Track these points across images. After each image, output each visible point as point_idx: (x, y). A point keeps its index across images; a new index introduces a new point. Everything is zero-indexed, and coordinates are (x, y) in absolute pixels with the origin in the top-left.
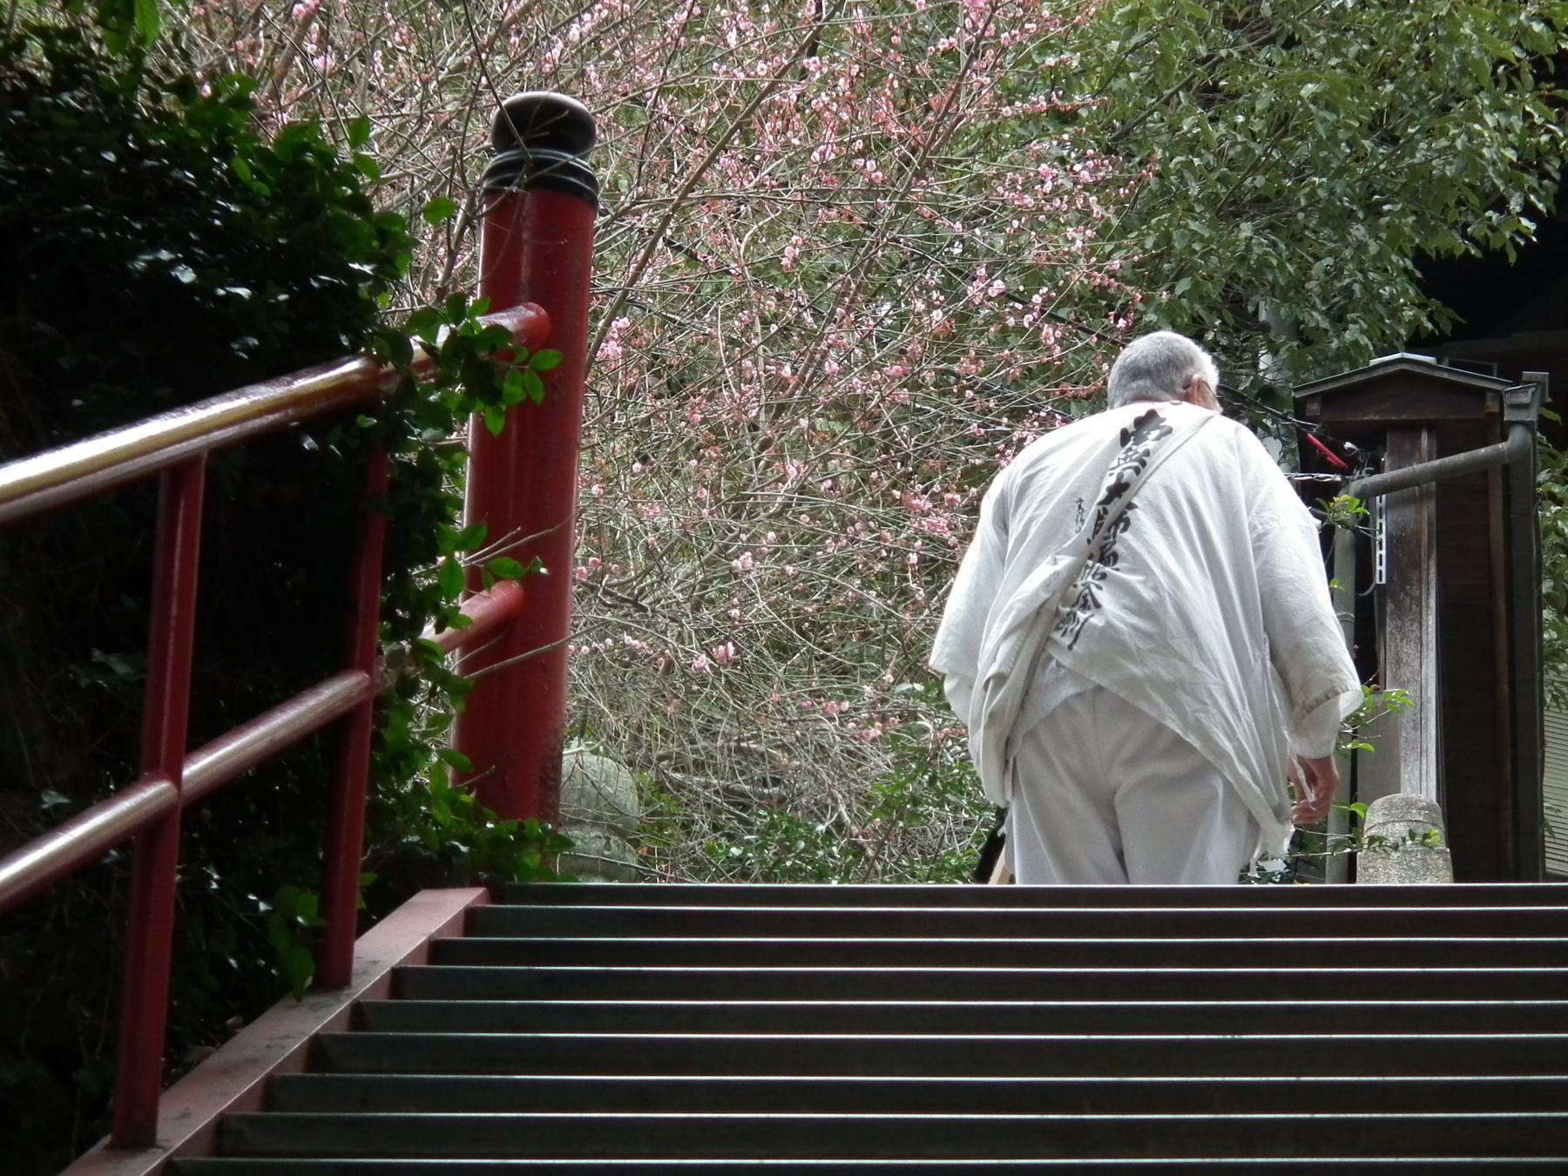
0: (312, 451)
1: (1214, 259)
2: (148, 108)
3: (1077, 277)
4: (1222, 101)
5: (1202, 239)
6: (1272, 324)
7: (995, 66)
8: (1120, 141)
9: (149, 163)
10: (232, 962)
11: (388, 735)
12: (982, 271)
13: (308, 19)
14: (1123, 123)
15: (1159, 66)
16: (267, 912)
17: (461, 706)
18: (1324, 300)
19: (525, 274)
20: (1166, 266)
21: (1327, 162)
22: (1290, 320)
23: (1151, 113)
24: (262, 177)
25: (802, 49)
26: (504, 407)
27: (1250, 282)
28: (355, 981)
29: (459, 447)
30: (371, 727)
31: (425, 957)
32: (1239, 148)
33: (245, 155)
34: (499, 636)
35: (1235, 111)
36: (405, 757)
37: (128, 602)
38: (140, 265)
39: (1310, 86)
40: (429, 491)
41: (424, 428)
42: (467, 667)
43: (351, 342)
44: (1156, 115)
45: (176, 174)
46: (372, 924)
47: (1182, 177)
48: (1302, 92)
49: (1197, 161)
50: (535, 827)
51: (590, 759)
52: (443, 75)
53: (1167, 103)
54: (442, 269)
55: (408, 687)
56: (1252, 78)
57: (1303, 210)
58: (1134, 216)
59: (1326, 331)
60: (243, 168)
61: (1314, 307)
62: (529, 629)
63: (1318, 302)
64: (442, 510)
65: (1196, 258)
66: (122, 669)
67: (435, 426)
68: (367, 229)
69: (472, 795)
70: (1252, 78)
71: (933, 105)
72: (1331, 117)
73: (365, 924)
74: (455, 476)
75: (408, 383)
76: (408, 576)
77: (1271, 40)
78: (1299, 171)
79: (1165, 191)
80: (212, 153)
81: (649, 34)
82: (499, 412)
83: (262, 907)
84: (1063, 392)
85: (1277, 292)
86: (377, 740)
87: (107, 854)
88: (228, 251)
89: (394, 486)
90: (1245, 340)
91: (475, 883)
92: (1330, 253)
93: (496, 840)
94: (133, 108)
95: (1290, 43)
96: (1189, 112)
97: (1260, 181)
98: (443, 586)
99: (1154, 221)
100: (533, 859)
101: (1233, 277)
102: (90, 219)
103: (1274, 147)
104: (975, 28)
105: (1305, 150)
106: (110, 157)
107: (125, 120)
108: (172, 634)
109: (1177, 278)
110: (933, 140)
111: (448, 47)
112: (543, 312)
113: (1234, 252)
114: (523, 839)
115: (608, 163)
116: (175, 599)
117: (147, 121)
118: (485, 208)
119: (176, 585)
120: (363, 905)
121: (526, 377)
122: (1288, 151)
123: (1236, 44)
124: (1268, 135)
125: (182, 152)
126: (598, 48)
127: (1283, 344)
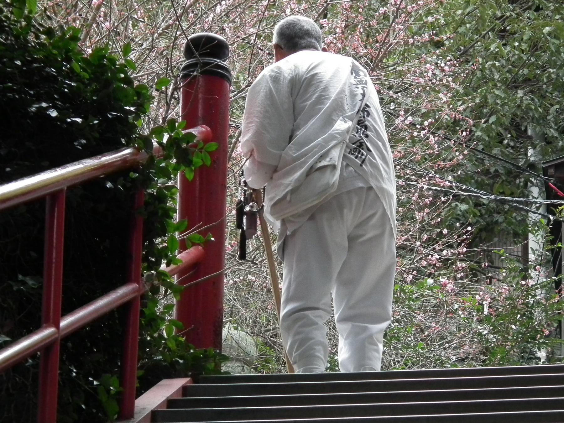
0: (110, 188)
1: (506, 107)
2: (34, 42)
3: (445, 117)
4: (508, 36)
5: (501, 98)
6: (533, 136)
7: (405, 21)
8: (464, 55)
9: (35, 65)
10: (83, 406)
11: (147, 311)
12: (402, 113)
13: (99, 7)
14: (464, 47)
15: (480, 21)
16: (97, 385)
17: (179, 298)
18: (556, 124)
19: (200, 112)
20: (485, 110)
21: (555, 62)
22: (541, 133)
23: (477, 42)
24: (85, 70)
25: (319, 15)
26: (193, 168)
27: (523, 117)
28: (135, 416)
29: (173, 187)
30: (139, 308)
31: (166, 406)
32: (516, 57)
33: (78, 61)
34: (193, 269)
35: (514, 40)
36: (153, 322)
37: (33, 254)
38: (33, 109)
39: (547, 28)
40: (163, 205)
41: (159, 178)
42: (180, 283)
43: (126, 141)
44: (479, 43)
45: (48, 69)
46: (142, 394)
47: (491, 71)
48: (544, 31)
49: (497, 64)
50: (212, 351)
51: (234, 332)
52: (160, 31)
53: (484, 37)
54: (163, 111)
55: (155, 290)
56: (521, 25)
57: (545, 84)
58: (470, 89)
59: (557, 138)
60: (77, 66)
61: (551, 127)
62: (209, 264)
63: (553, 125)
64: (167, 213)
65: (499, 107)
66: (30, 282)
67: (164, 177)
68: (131, 92)
69: (184, 338)
70: (521, 25)
71: (379, 39)
72: (557, 42)
73: (139, 393)
74: (173, 199)
75: (152, 158)
76: (154, 243)
77: (529, 8)
78: (543, 67)
79: (484, 77)
80: (63, 60)
81: (251, 12)
82: (192, 170)
83: (95, 383)
84: (439, 165)
85: (535, 121)
86: (142, 314)
87: (27, 361)
88: (72, 102)
89: (147, 204)
90: (521, 143)
91: (186, 376)
92: (558, 103)
93: (195, 358)
94: (27, 41)
95: (538, 9)
96: (494, 41)
97: (526, 71)
98: (170, 247)
99: (479, 91)
100: (211, 365)
101: (515, 115)
102: (11, 90)
103: (532, 56)
104: (396, 4)
105: (545, 57)
106: (18, 63)
107: (24, 46)
108: (54, 265)
109: (490, 116)
110: (379, 55)
111: (162, 18)
112: (209, 129)
113: (516, 103)
114: (207, 357)
115: (234, 65)
116: (54, 251)
117: (34, 47)
118: (182, 84)
119: (54, 245)
120: (138, 385)
121: (203, 154)
122: (538, 57)
123: (513, 10)
124: (529, 51)
125: (49, 60)
126: (228, 17)
127: (538, 144)
